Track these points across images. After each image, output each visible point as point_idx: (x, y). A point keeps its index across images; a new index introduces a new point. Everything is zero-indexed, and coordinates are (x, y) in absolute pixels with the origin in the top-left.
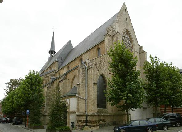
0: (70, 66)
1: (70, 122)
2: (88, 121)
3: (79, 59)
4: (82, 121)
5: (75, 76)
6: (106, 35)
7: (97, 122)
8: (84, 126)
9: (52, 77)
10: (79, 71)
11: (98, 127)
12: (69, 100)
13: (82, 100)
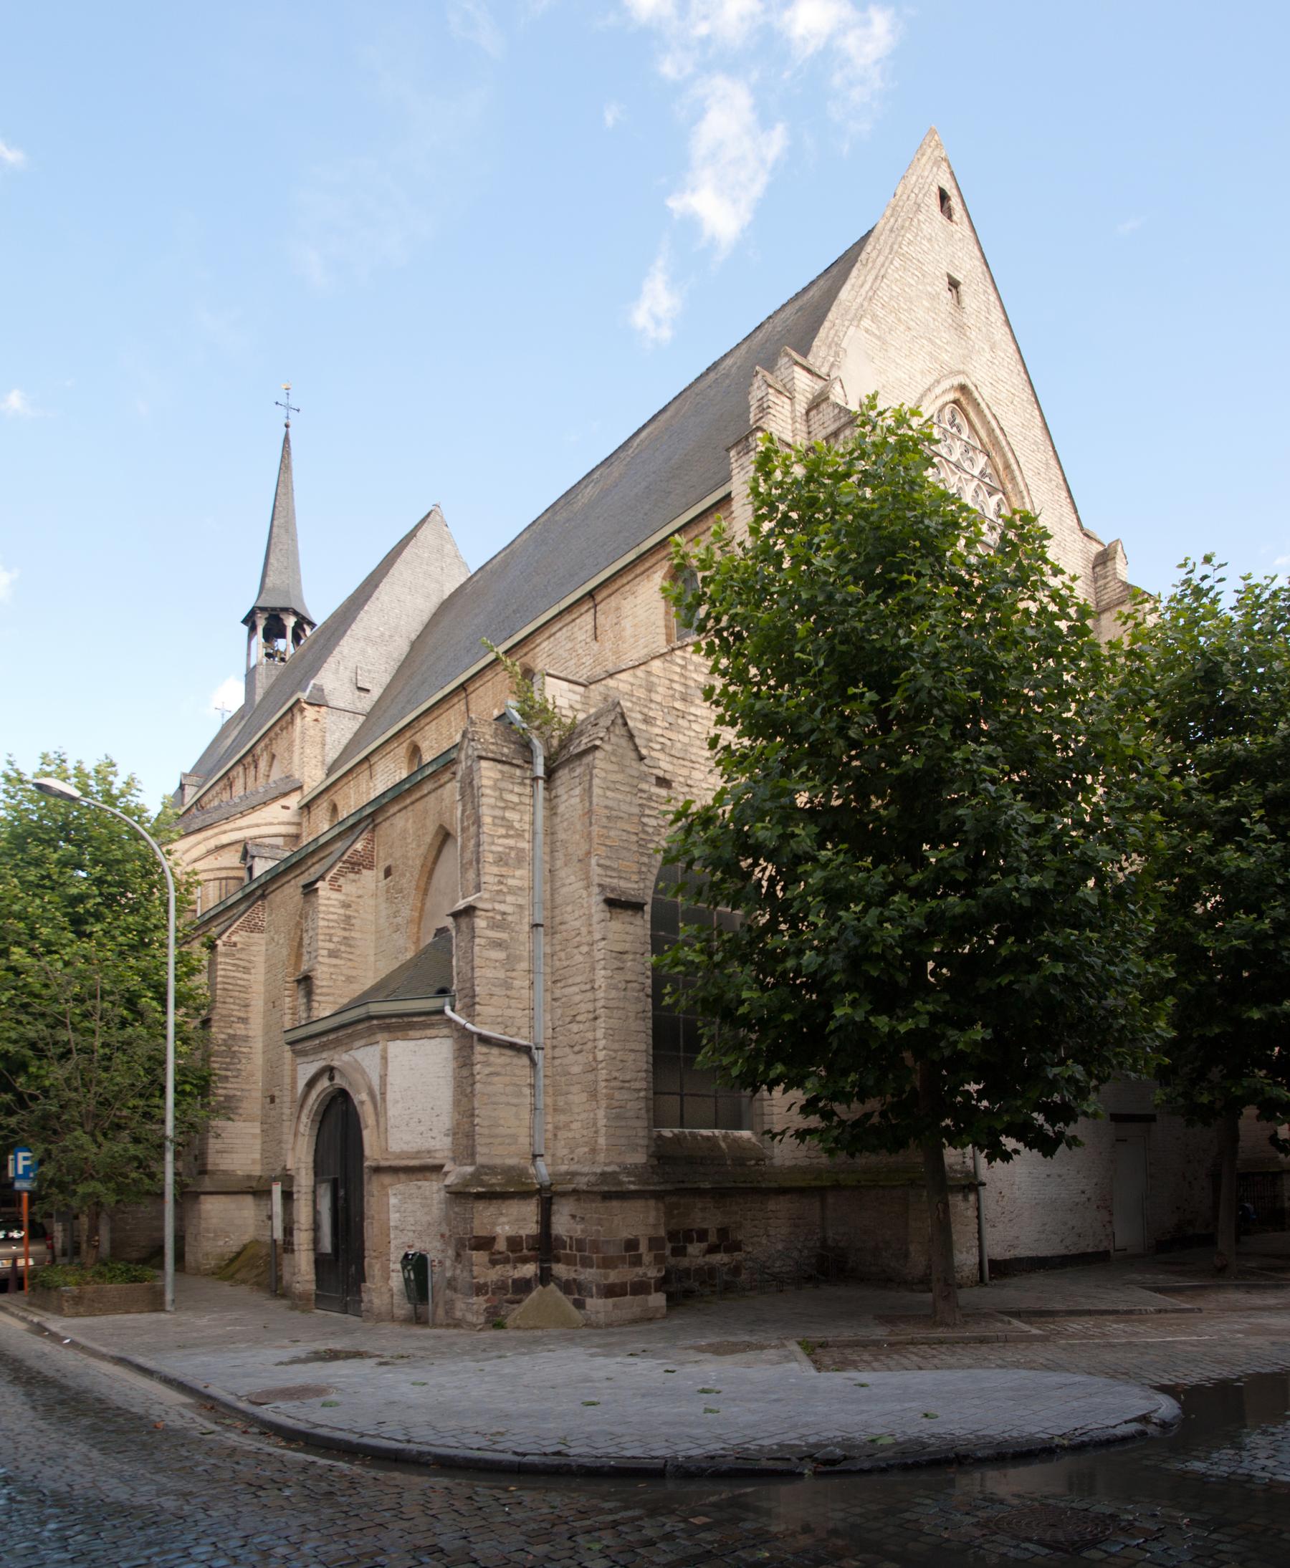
1: (396, 1256)
4: (501, 1245)
7: (647, 1258)
8: (523, 1287)
11: (657, 1300)
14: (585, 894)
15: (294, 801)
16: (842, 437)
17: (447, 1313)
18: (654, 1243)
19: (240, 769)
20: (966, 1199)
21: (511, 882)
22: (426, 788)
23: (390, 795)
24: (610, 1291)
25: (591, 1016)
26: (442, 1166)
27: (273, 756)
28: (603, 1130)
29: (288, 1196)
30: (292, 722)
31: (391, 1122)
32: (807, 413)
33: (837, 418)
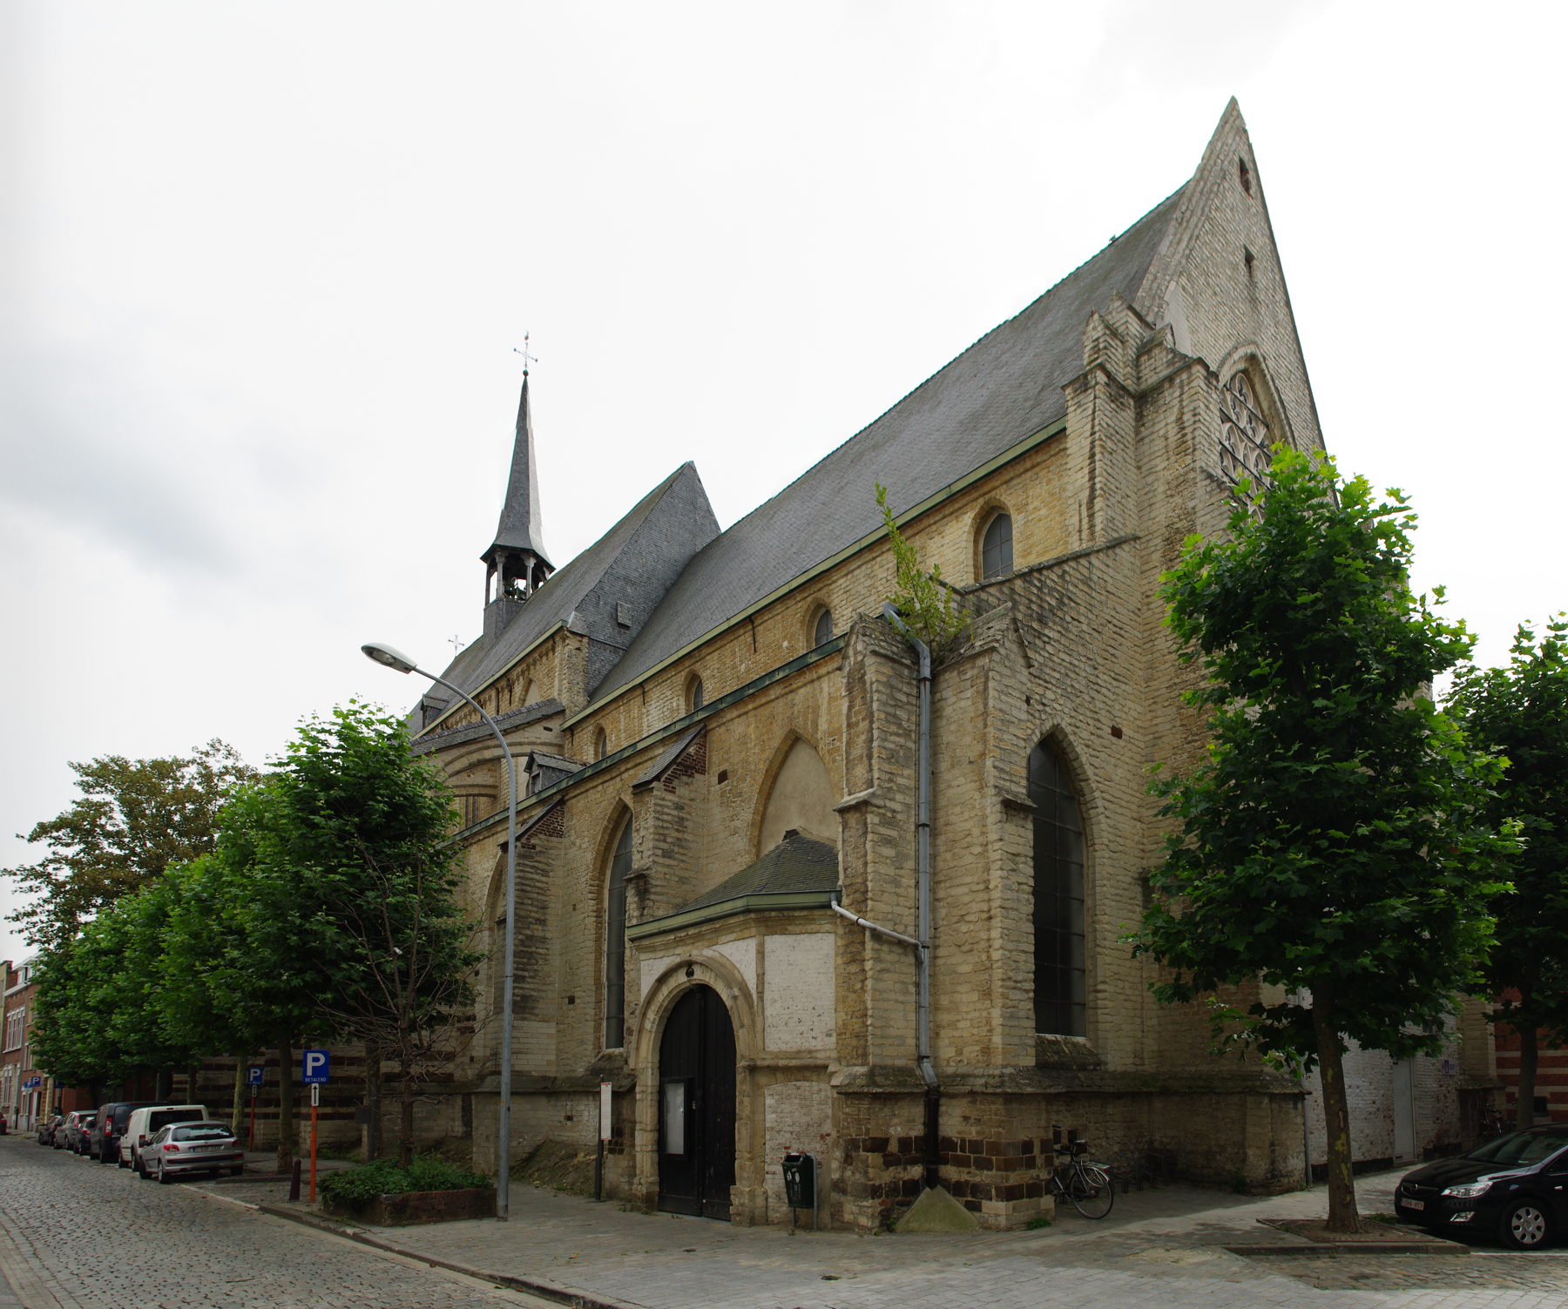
0: (705, 675)
2: (949, 1143)
3: (799, 608)
4: (893, 1147)
5: (794, 740)
6: (1082, 383)
7: (1040, 1160)
8: (912, 1189)
9: (539, 760)
10: (856, 682)
11: (1047, 1202)
12: (761, 953)
13: (890, 956)
14: (977, 796)
15: (555, 724)
16: (1178, 381)
17: (833, 1215)
18: (1046, 1146)
19: (493, 693)
20: (1296, 1107)
21: (900, 780)
22: (772, 694)
23: (729, 700)
24: (1010, 1194)
25: (985, 916)
26: (826, 1067)
27: (530, 682)
28: (999, 1030)
29: (622, 1096)
30: (553, 649)
31: (769, 1021)
32: (1138, 357)
33: (1170, 363)
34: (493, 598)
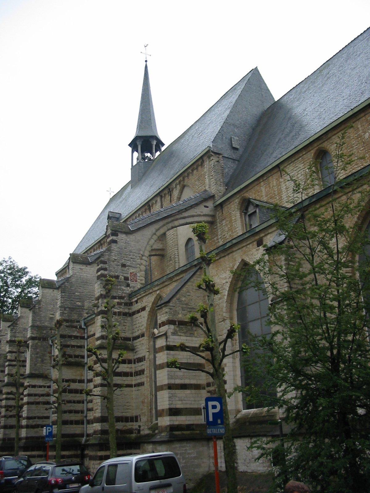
15: (210, 204)
34: (135, 162)
